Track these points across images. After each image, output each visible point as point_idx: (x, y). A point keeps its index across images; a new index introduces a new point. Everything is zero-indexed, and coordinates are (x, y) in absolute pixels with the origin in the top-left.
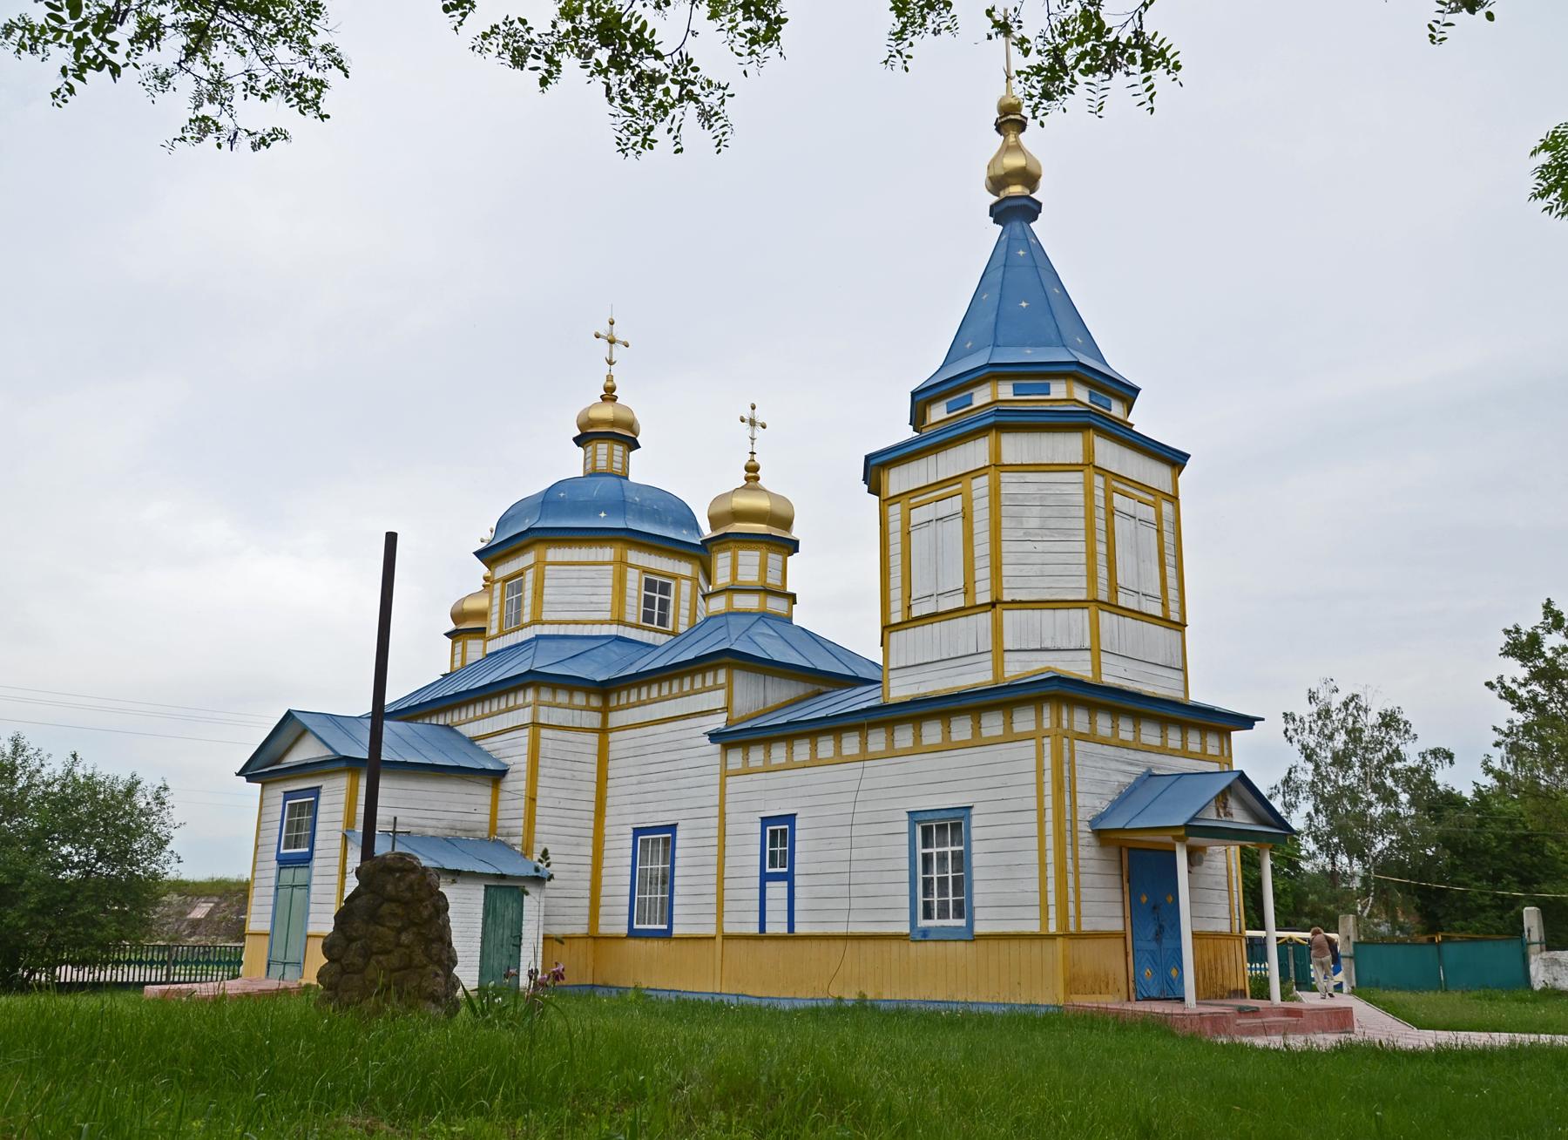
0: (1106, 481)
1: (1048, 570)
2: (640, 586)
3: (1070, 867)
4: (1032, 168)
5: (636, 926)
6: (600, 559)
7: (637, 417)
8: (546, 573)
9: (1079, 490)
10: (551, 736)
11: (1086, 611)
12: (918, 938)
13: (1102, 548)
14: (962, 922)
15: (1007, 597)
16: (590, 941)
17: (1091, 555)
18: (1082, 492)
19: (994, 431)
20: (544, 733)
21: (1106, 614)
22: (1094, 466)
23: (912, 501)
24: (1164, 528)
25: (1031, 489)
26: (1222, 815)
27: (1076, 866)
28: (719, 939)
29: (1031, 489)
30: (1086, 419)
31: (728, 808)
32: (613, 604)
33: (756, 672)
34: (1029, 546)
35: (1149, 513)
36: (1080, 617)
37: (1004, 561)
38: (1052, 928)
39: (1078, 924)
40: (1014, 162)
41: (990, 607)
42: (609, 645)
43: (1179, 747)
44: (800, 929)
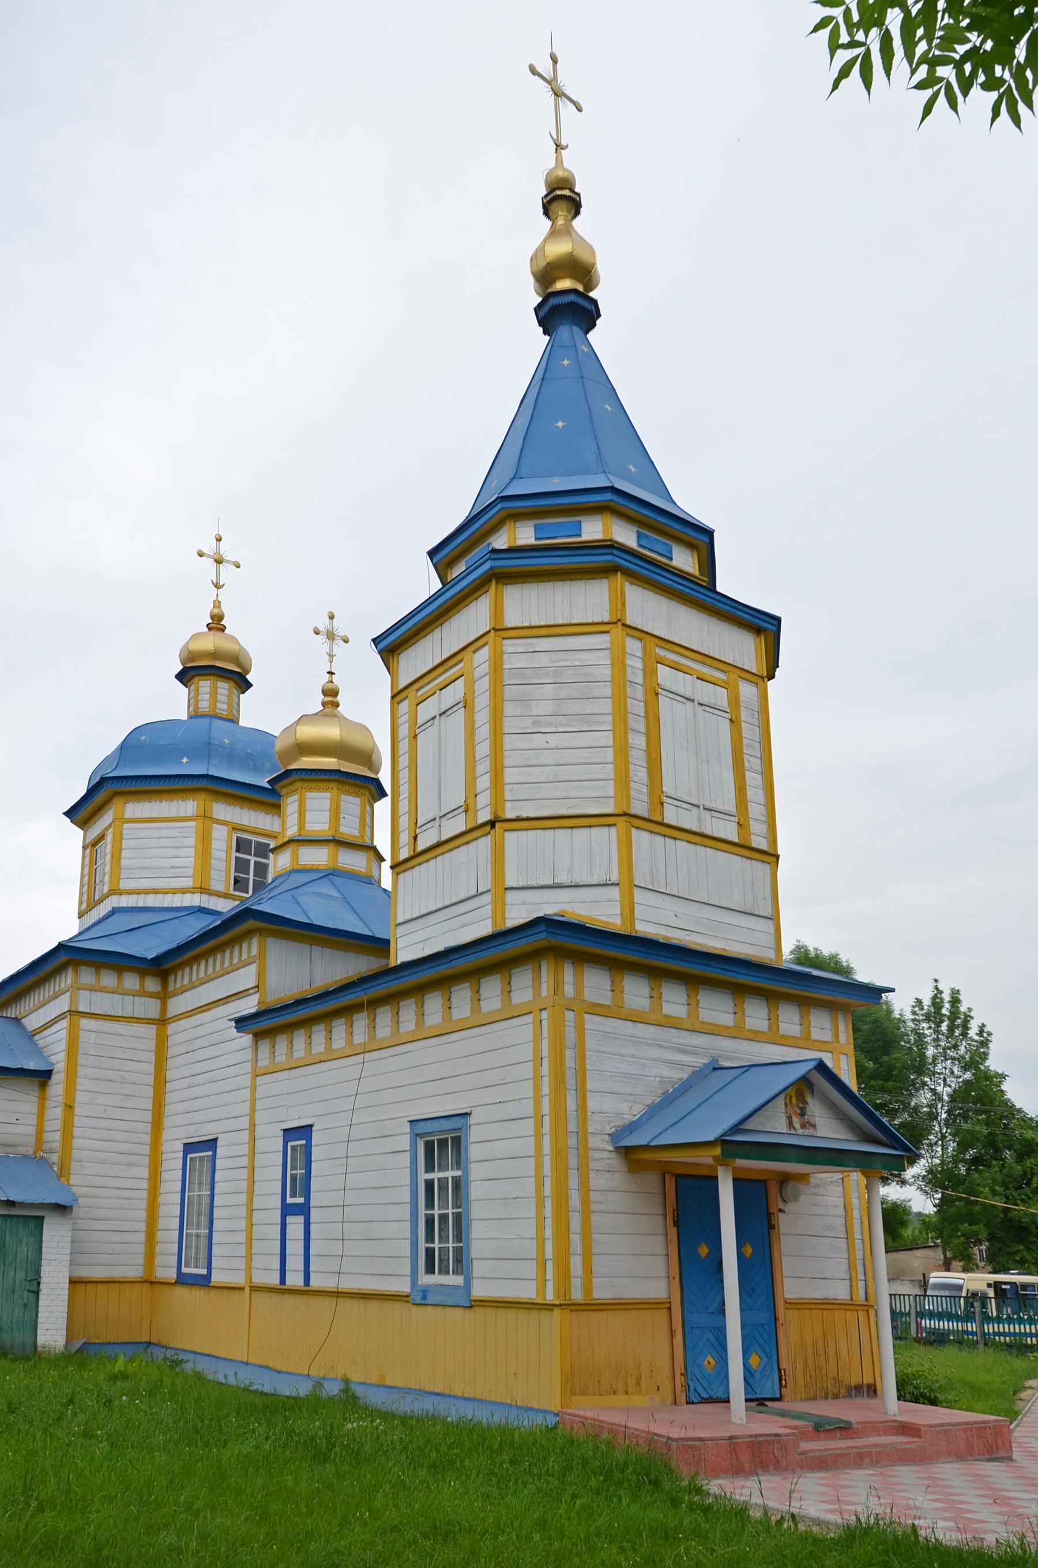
0: (645, 647)
1: (564, 772)
2: (229, 847)
3: (575, 1200)
4: (583, 255)
5: (184, 1270)
6: (182, 814)
7: (245, 644)
8: (124, 832)
9: (604, 658)
10: (94, 1028)
11: (613, 830)
12: (419, 1301)
13: (638, 741)
14: (458, 1280)
15: (510, 814)
16: (146, 1287)
17: (622, 750)
18: (608, 662)
19: (494, 582)
20: (85, 1023)
21: (645, 835)
22: (623, 625)
23: (420, 693)
24: (743, 718)
25: (543, 660)
26: (797, 1126)
27: (585, 1201)
28: (247, 1290)
29: (543, 660)
30: (610, 558)
31: (259, 1117)
32: (195, 868)
33: (287, 939)
34: (539, 740)
35: (720, 696)
36: (605, 839)
37: (507, 762)
38: (550, 1297)
39: (588, 1288)
40: (560, 248)
41: (488, 827)
42: (188, 918)
43: (766, 1029)
44: (316, 1282)
